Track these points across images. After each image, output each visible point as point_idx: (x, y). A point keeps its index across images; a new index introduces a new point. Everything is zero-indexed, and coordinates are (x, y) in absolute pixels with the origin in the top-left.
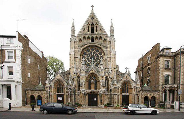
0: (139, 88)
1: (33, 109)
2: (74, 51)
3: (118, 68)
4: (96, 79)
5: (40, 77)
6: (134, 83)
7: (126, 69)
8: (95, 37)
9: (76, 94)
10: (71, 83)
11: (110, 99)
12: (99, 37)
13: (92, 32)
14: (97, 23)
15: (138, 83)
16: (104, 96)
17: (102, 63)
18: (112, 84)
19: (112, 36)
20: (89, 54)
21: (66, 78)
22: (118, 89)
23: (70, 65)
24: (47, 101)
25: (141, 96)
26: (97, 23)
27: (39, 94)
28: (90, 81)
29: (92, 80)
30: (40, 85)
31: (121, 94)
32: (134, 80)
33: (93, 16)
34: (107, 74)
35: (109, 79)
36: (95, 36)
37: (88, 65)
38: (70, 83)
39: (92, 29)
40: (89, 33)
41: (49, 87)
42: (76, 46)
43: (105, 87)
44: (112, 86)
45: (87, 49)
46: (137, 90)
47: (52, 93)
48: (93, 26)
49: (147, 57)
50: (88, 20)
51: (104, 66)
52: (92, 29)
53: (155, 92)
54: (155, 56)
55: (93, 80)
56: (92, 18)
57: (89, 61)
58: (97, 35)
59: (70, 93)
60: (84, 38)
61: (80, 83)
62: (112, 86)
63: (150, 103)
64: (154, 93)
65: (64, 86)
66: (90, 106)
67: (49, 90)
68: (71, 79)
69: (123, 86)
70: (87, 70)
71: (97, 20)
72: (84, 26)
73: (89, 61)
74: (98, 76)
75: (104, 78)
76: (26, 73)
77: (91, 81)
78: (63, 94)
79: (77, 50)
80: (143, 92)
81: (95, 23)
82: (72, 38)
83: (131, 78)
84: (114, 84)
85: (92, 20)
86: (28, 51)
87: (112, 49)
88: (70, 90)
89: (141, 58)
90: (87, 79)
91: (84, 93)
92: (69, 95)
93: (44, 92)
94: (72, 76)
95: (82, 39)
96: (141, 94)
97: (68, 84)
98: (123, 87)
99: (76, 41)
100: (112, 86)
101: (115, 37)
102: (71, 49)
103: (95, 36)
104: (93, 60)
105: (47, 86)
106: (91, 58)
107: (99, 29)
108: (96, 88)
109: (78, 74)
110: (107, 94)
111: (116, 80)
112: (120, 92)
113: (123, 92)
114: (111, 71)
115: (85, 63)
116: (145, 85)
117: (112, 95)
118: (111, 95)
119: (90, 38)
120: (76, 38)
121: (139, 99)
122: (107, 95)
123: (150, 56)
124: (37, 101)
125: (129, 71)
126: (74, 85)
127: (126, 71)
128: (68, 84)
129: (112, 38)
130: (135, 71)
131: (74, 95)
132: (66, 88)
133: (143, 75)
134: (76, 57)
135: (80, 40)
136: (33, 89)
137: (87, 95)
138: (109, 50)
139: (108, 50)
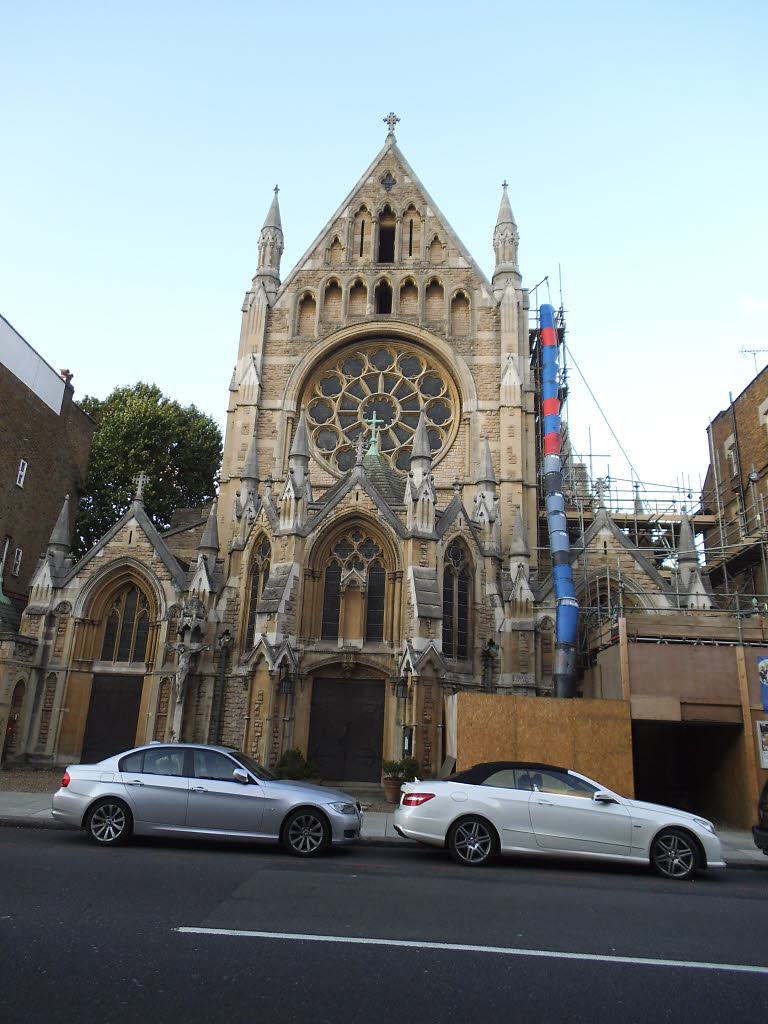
2: (263, 372)
4: (377, 562)
8: (395, 284)
10: (206, 586)
12: (420, 283)
13: (385, 254)
14: (412, 207)
19: (508, 273)
20: (355, 389)
26: (412, 207)
28: (333, 573)
33: (390, 171)
34: (460, 527)
35: (478, 562)
38: (201, 583)
39: (386, 239)
40: (361, 260)
44: (503, 621)
48: (388, 223)
50: (361, 189)
52: (386, 239)
55: (360, 567)
56: (387, 181)
58: (411, 273)
59: (183, 662)
60: (333, 288)
62: (498, 612)
65: (158, 609)
67: (47, 636)
71: (418, 189)
72: (335, 222)
75: (437, 551)
77: (345, 574)
78: (140, 669)
81: (398, 207)
82: (261, 294)
84: (516, 608)
85: (383, 191)
89: (722, 414)
92: (179, 679)
95: (317, 294)
97: (183, 593)
102: (240, 356)
103: (395, 283)
105: (36, 604)
107: (422, 238)
108: (373, 630)
109: (263, 522)
119: (365, 289)
126: (223, 604)
131: (222, 682)
132: (164, 626)
135: (307, 301)
137: (309, 686)
138: (485, 360)
139: (478, 360)
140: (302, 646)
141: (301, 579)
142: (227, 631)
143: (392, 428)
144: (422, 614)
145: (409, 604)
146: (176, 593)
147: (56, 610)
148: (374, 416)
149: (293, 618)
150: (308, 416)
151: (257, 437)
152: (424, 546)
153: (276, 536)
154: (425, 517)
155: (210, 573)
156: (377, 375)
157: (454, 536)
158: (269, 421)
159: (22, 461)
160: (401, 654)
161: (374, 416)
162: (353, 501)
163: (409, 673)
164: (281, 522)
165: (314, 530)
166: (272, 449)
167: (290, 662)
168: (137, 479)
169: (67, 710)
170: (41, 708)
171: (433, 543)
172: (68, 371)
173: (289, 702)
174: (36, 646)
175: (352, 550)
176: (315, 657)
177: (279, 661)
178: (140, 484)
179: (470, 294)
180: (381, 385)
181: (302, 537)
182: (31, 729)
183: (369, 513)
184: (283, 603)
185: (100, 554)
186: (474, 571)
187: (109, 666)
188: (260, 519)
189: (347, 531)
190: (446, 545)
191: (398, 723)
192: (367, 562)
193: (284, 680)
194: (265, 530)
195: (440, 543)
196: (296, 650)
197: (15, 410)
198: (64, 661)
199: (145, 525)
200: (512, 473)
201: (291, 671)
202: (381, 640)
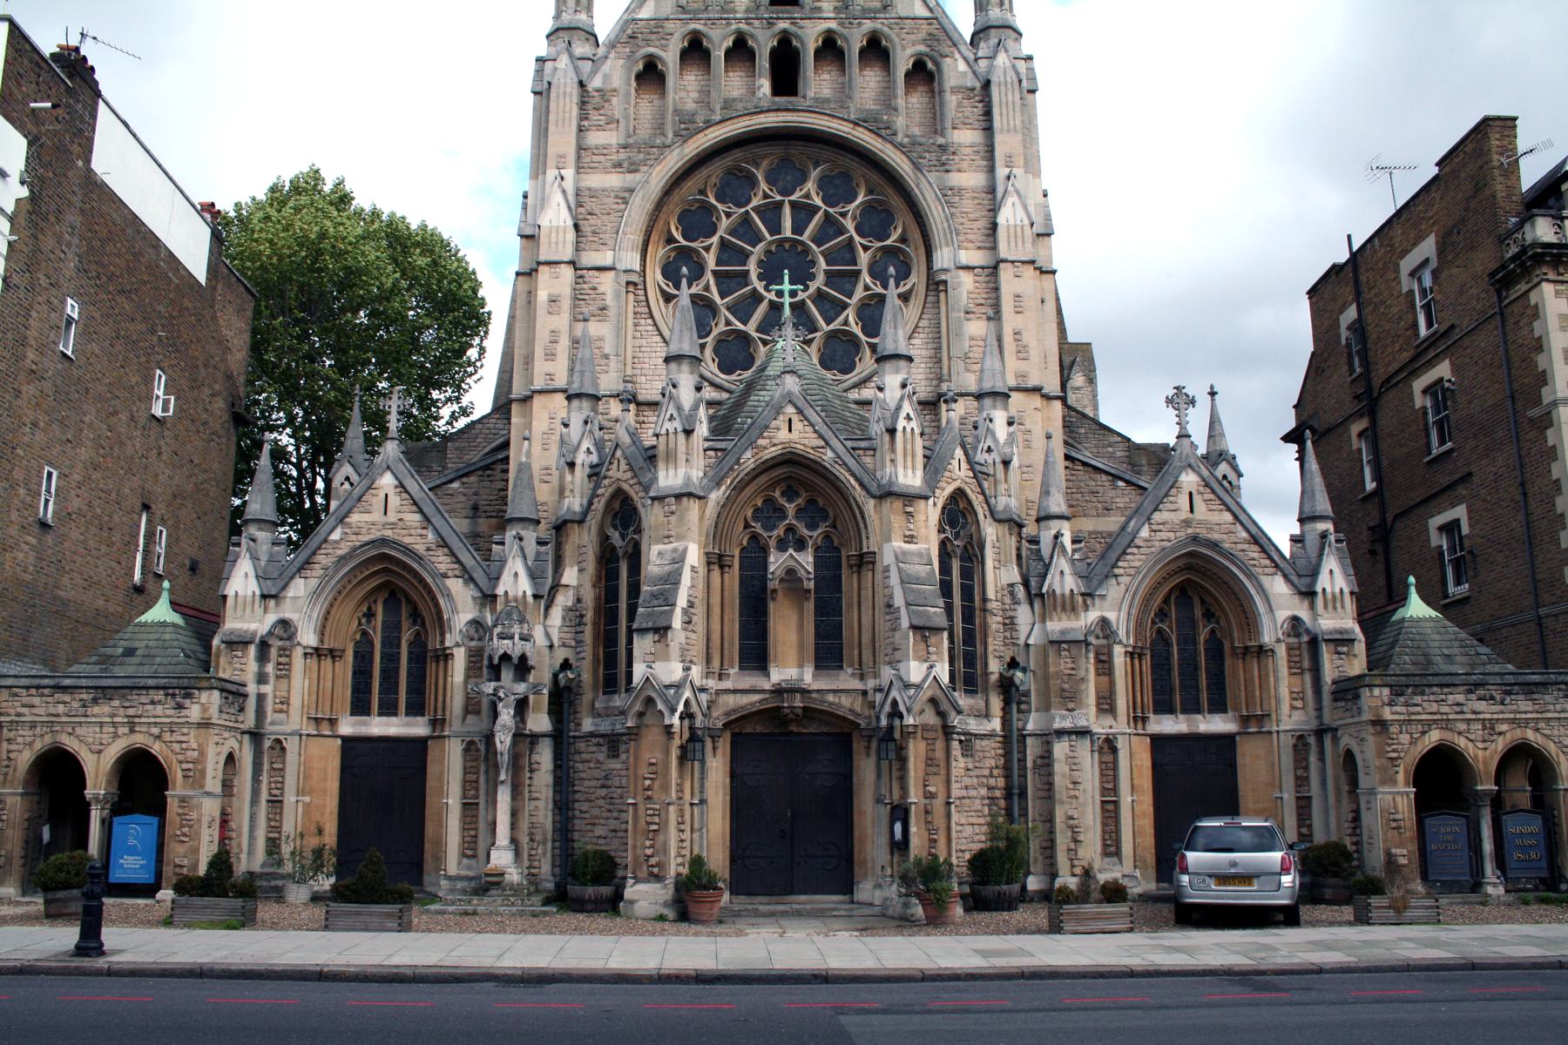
0: (1341, 641)
1: (90, 943)
3: (1091, 380)
5: (159, 508)
6: (1278, 587)
7: (1180, 400)
9: (588, 725)
10: (525, 586)
11: (1008, 796)
12: (855, 42)
15: (1323, 582)
16: (930, 761)
17: (894, 336)
18: (1020, 591)
20: (744, 228)
21: (462, 525)
22: (1104, 665)
23: (557, 17)
24: (224, 822)
25: (1381, 753)
27: (139, 740)
28: (755, 556)
29: (782, 546)
30: (161, 612)
31: (1139, 719)
32: (1286, 548)
34: (958, 474)
35: (990, 531)
36: (810, 36)
37: (735, 353)
38: (516, 582)
41: (264, 646)
42: (595, 138)
43: (940, 630)
45: (715, 171)
46: (1329, 674)
47: (290, 722)
49: (1408, 264)
51: (919, 375)
53: (1530, 689)
54: (1484, 260)
55: (800, 545)
57: (743, 310)
58: (833, 25)
59: (506, 716)
60: (695, 51)
61: (634, 590)
63: (1488, 846)
64: (1524, 705)
66: (762, 904)
67: (262, 679)
68: (530, 536)
69: (1162, 614)
70: (723, 425)
73: (743, 310)
74: (858, 492)
75: (930, 513)
76: (18, 474)
77: (777, 562)
78: (418, 728)
79: (614, 180)
80: (1397, 691)
82: (564, 62)
83: (1240, 516)
86: (72, 218)
87: (1001, 172)
88: (507, 675)
89: (1335, 270)
90: (719, 531)
91: (687, 715)
92: (503, 741)
93: (194, 712)
94: (544, 493)
95: (670, 56)
96: (1380, 724)
97: (488, 598)
98: (1159, 631)
99: (596, 83)
100: (1023, 614)
101: (1026, 47)
102: (539, 162)
103: (810, 36)
104: (787, 300)
106: (770, 275)
108: (828, 654)
109: (619, 473)
110: (973, 725)
111: (1067, 540)
112: (1122, 703)
113: (1164, 706)
114: (1001, 430)
115: (703, 330)
116: (1416, 607)
117: (1032, 748)
118: (1011, 740)
120: (601, 51)
121: (1354, 782)
122: (968, 740)
123: (1427, 247)
124: (107, 826)
125: (1214, 422)
127: (1183, 435)
128: (488, 598)
129: (1002, 59)
130: (1290, 423)
133: (1377, 477)
134: (590, 258)
135: (651, 75)
136: (85, 669)
137: (724, 744)
138: (969, 178)
139: (956, 179)
140: (712, 683)
141: (702, 571)
142: (566, 661)
143: (809, 297)
144: (915, 622)
145: (889, 606)
146: (474, 598)
147: (270, 633)
148: (786, 278)
149: (693, 636)
150: (659, 277)
151: (578, 318)
152: (909, 509)
153: (653, 499)
154: (909, 459)
155: (530, 563)
156: (780, 205)
157: (949, 489)
158: (595, 289)
159: (158, 372)
160: (880, 690)
161: (786, 278)
162: (783, 435)
163: (897, 722)
164: (661, 474)
165: (718, 485)
166: (601, 339)
167: (695, 708)
168: (388, 403)
169: (307, 799)
170: (264, 796)
171: (922, 502)
172: (213, 205)
173: (697, 775)
174: (246, 696)
175: (785, 517)
176: (731, 701)
177: (681, 708)
178: (394, 410)
179: (937, 64)
180: (787, 223)
181: (700, 498)
182: (252, 837)
183: (812, 455)
184: (678, 612)
185: (335, 536)
186: (982, 547)
187: (365, 724)
188: (614, 466)
189: (773, 485)
190: (940, 506)
191: (879, 801)
192: (815, 535)
193: (689, 740)
194: (625, 487)
195: (931, 501)
196: (703, 690)
197: (145, 283)
198: (296, 720)
199: (411, 484)
200: (1022, 376)
201: (698, 724)
202: (841, 668)
